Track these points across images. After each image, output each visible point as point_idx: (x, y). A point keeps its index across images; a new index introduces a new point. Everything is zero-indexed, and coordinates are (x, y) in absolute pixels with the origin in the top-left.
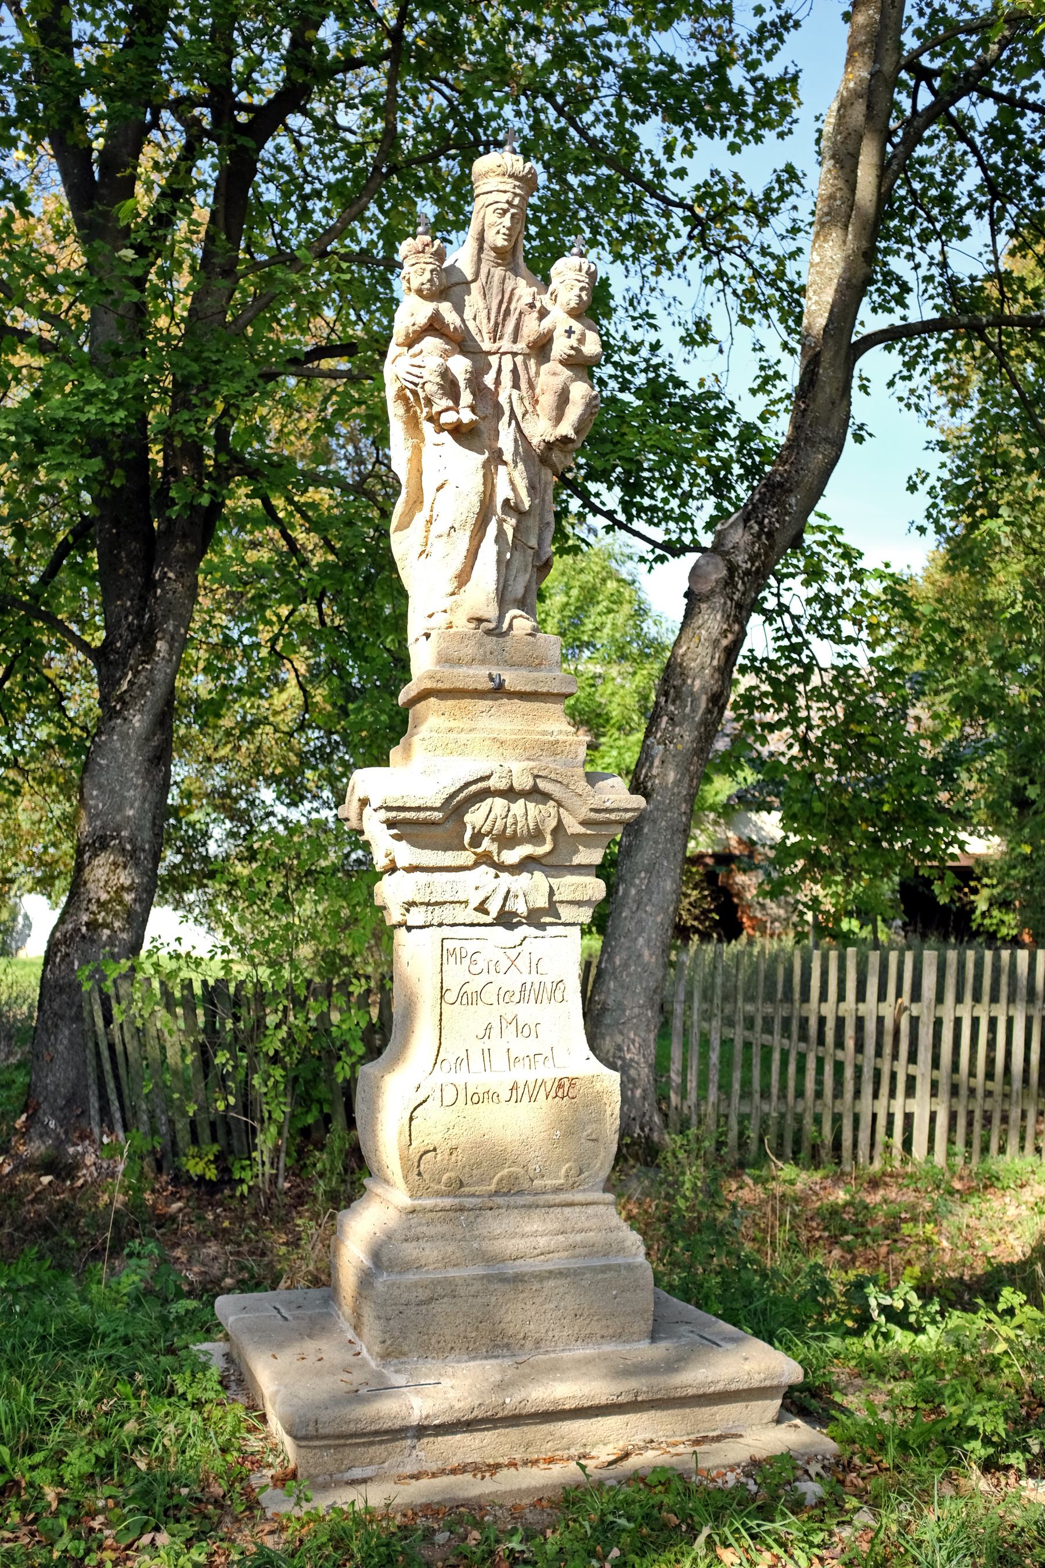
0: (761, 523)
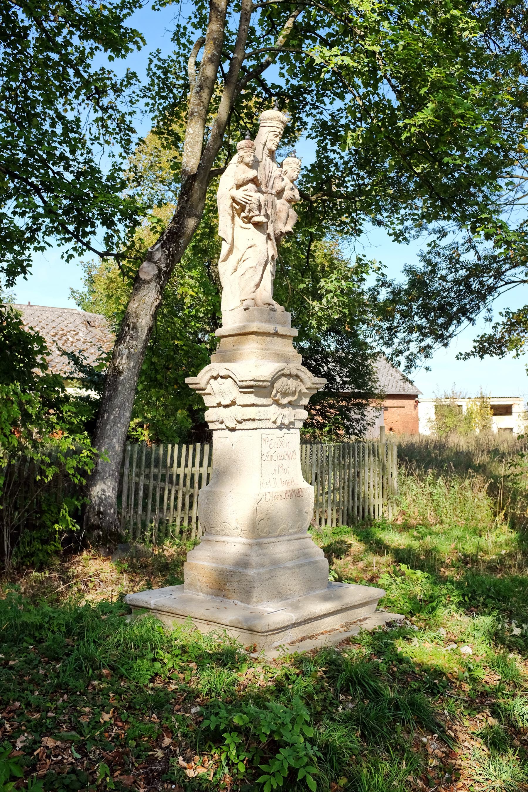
0: (169, 250)
